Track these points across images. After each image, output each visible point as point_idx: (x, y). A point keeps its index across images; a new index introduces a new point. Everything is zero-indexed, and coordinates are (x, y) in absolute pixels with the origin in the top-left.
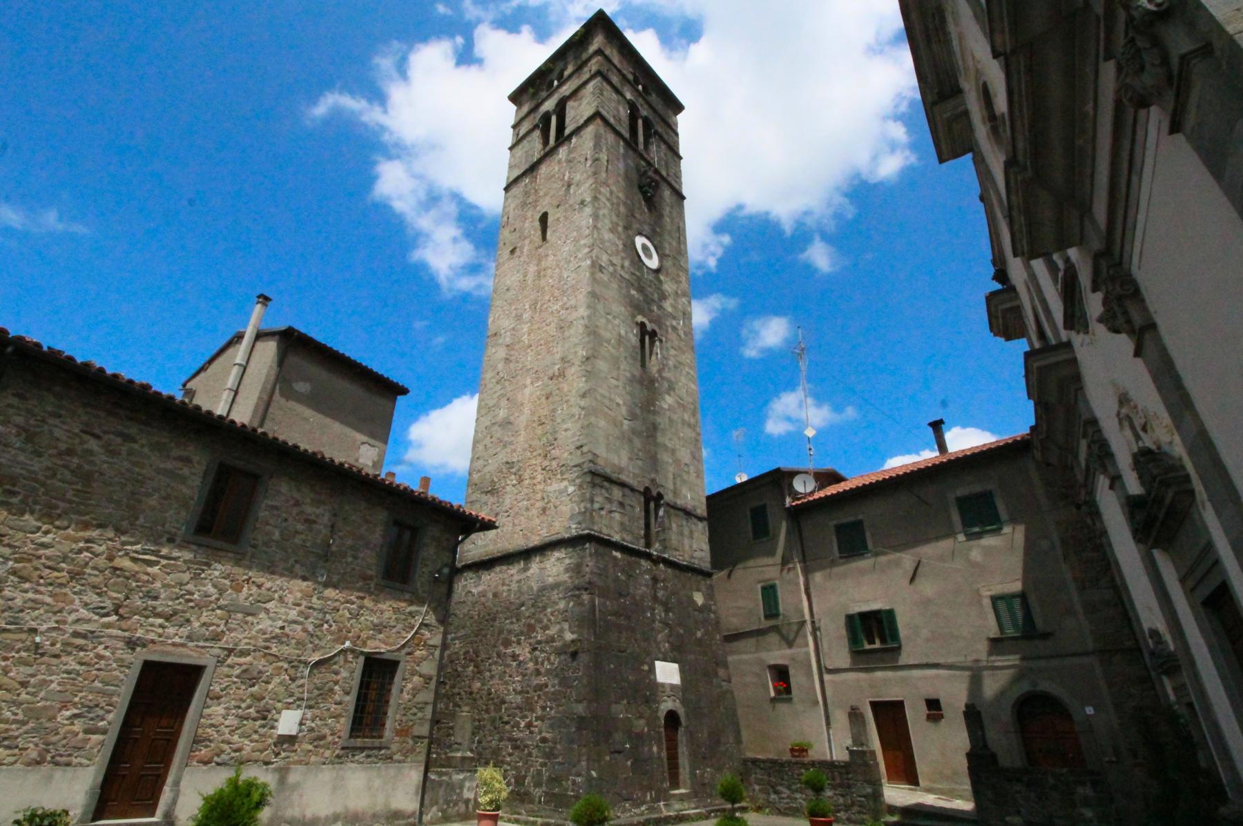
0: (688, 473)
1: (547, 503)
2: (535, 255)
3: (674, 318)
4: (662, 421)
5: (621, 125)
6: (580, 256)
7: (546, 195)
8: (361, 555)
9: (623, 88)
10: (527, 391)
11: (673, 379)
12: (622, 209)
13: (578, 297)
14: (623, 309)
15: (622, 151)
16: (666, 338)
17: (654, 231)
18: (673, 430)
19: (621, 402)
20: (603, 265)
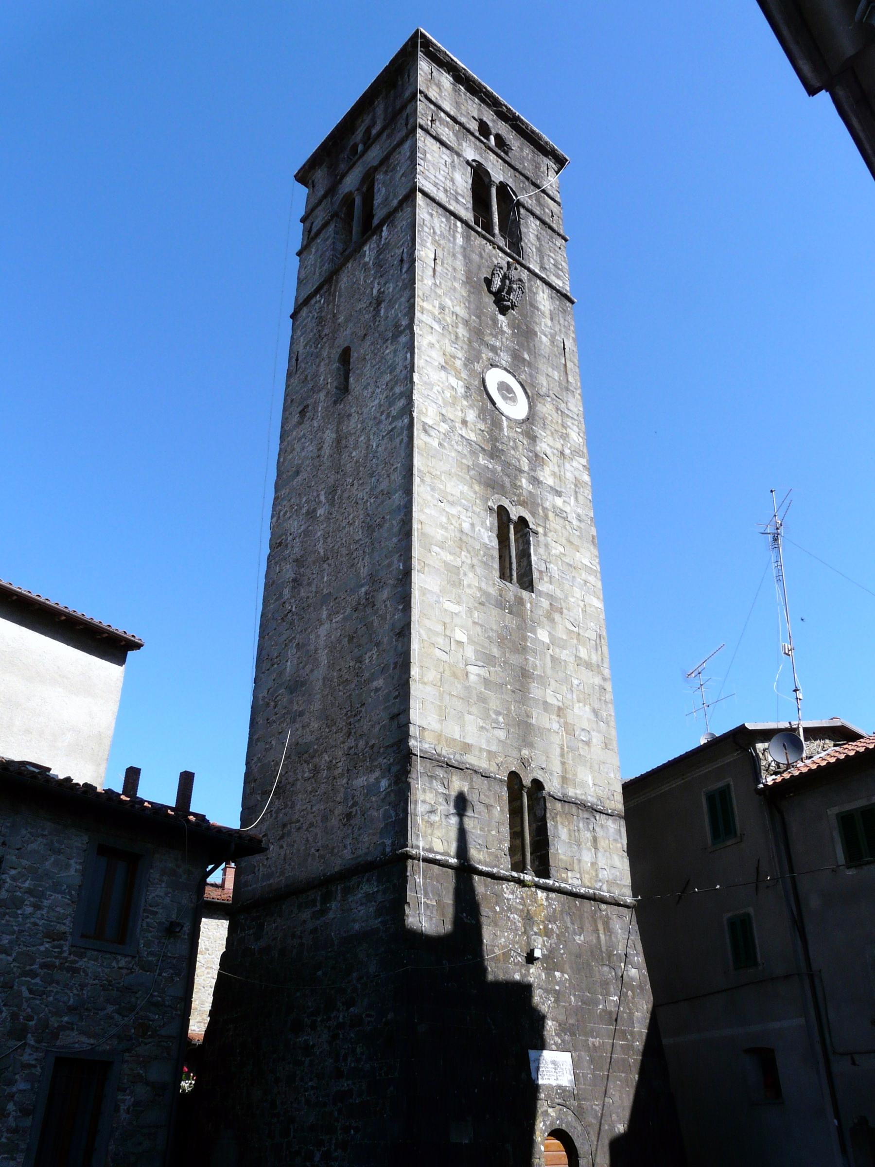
0: (588, 743)
1: (351, 807)
2: (334, 413)
3: (559, 494)
4: (538, 664)
8: (46, 903)
9: (460, 144)
10: (323, 631)
11: (559, 594)
12: (462, 331)
13: (392, 477)
14: (466, 488)
15: (460, 240)
16: (545, 527)
17: (516, 357)
18: (561, 675)
19: (464, 639)
20: (430, 422)
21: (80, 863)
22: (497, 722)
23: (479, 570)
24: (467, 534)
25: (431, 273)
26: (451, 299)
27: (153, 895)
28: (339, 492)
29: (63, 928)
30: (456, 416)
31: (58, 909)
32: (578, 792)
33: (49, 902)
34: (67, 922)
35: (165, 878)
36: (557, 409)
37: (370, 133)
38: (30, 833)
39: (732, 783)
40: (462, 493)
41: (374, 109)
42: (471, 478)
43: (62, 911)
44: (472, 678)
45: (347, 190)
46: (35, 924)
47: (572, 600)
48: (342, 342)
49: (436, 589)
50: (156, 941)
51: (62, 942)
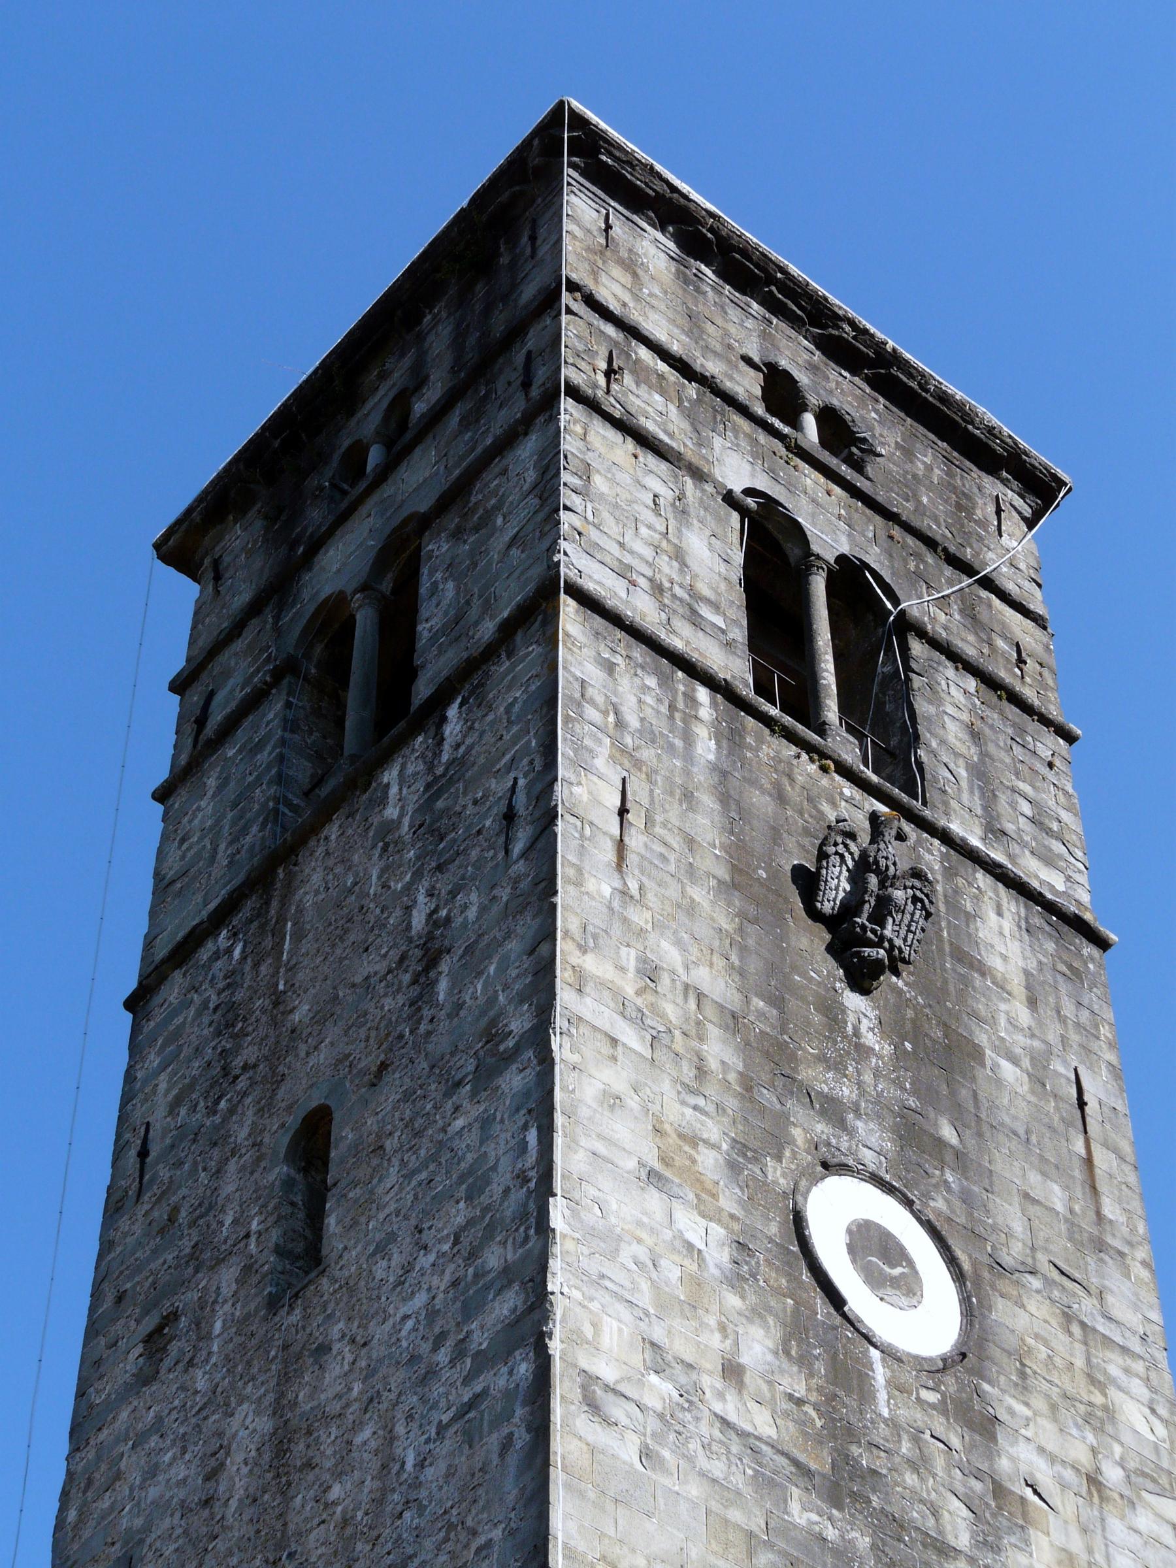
5: (695, 620)
6: (480, 1340)
7: (321, 1018)
15: (706, 748)
20: (608, 1372)
25: (608, 854)
26: (678, 943)
36: (1068, 1317)
41: (421, 338)
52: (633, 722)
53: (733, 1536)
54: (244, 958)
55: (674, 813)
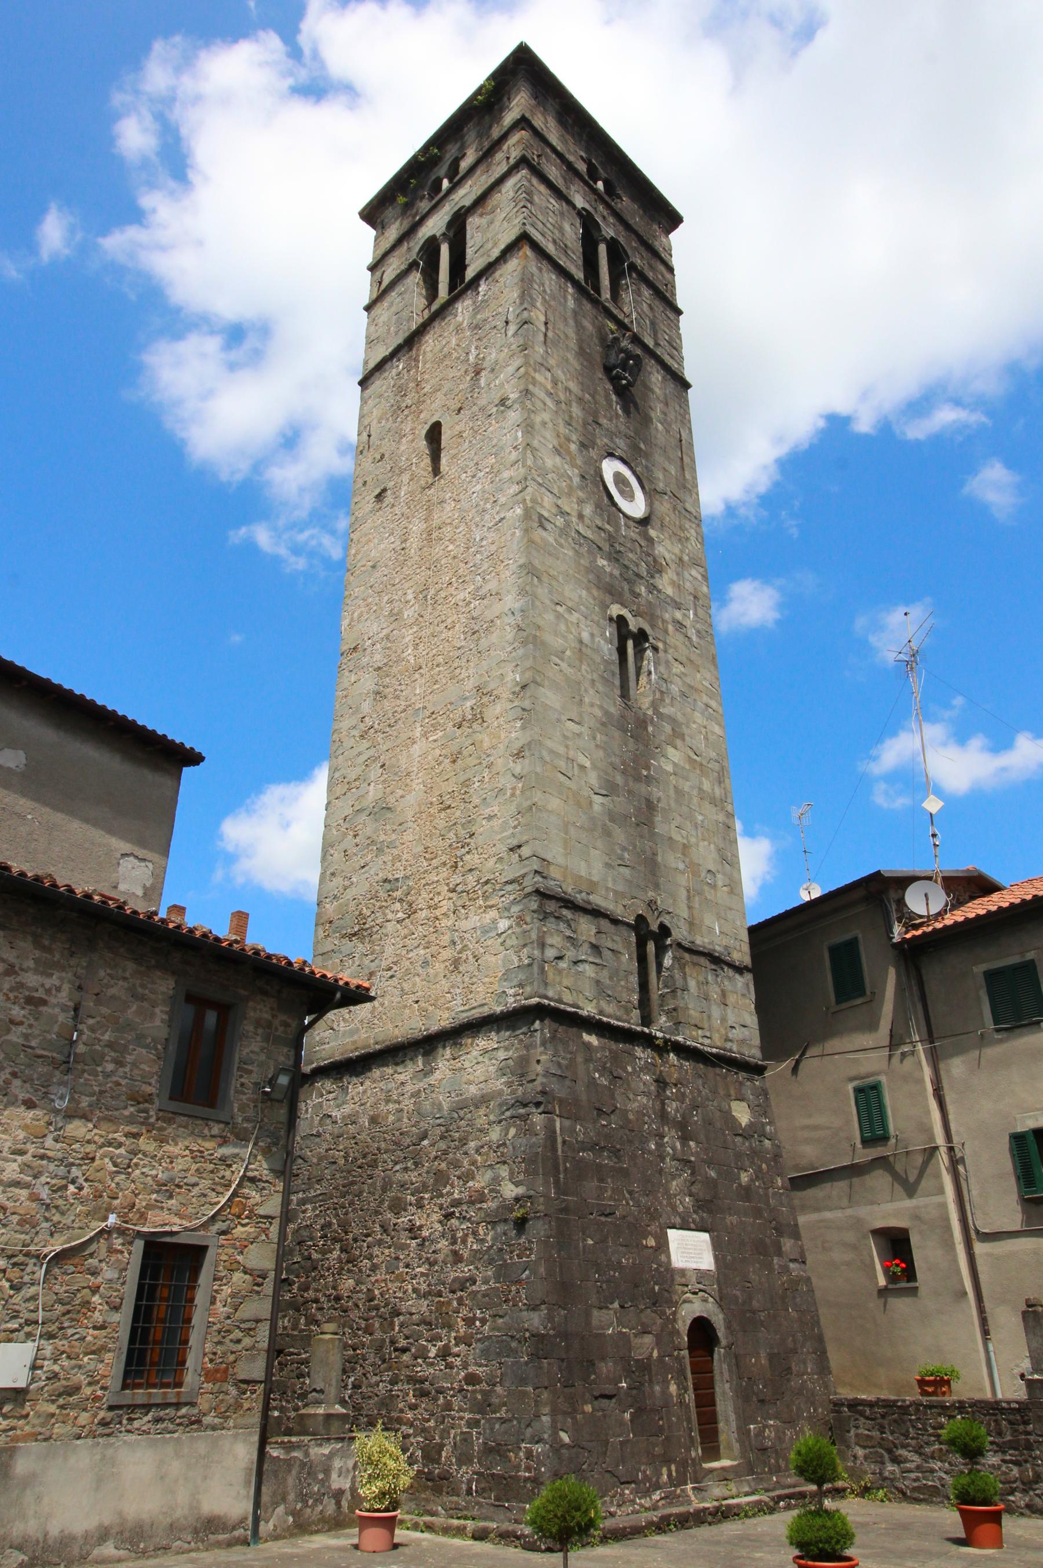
0: (714, 886)
1: (460, 953)
3: (678, 606)
8: (129, 1058)
9: (568, 188)
10: (416, 750)
11: (680, 717)
12: (576, 410)
14: (584, 593)
15: (571, 303)
16: (665, 643)
18: (685, 809)
20: (546, 514)
21: (166, 1013)
22: (622, 858)
23: (601, 688)
24: (587, 646)
25: (541, 338)
26: (563, 372)
27: (247, 1050)
28: (432, 592)
29: (149, 1089)
30: (572, 509)
31: (143, 1066)
32: (706, 940)
33: (133, 1057)
34: (153, 1081)
35: (260, 1031)
36: (675, 509)
37: (458, 166)
38: (109, 974)
39: (860, 936)
40: (580, 597)
41: (462, 137)
42: (590, 581)
43: (147, 1069)
44: (596, 808)
45: (429, 234)
46: (118, 1084)
47: (694, 726)
48: (428, 418)
49: (557, 706)
50: (252, 1105)
51: (147, 1105)
52: (549, 292)
53: (582, 568)
54: (403, 369)
55: (561, 326)
